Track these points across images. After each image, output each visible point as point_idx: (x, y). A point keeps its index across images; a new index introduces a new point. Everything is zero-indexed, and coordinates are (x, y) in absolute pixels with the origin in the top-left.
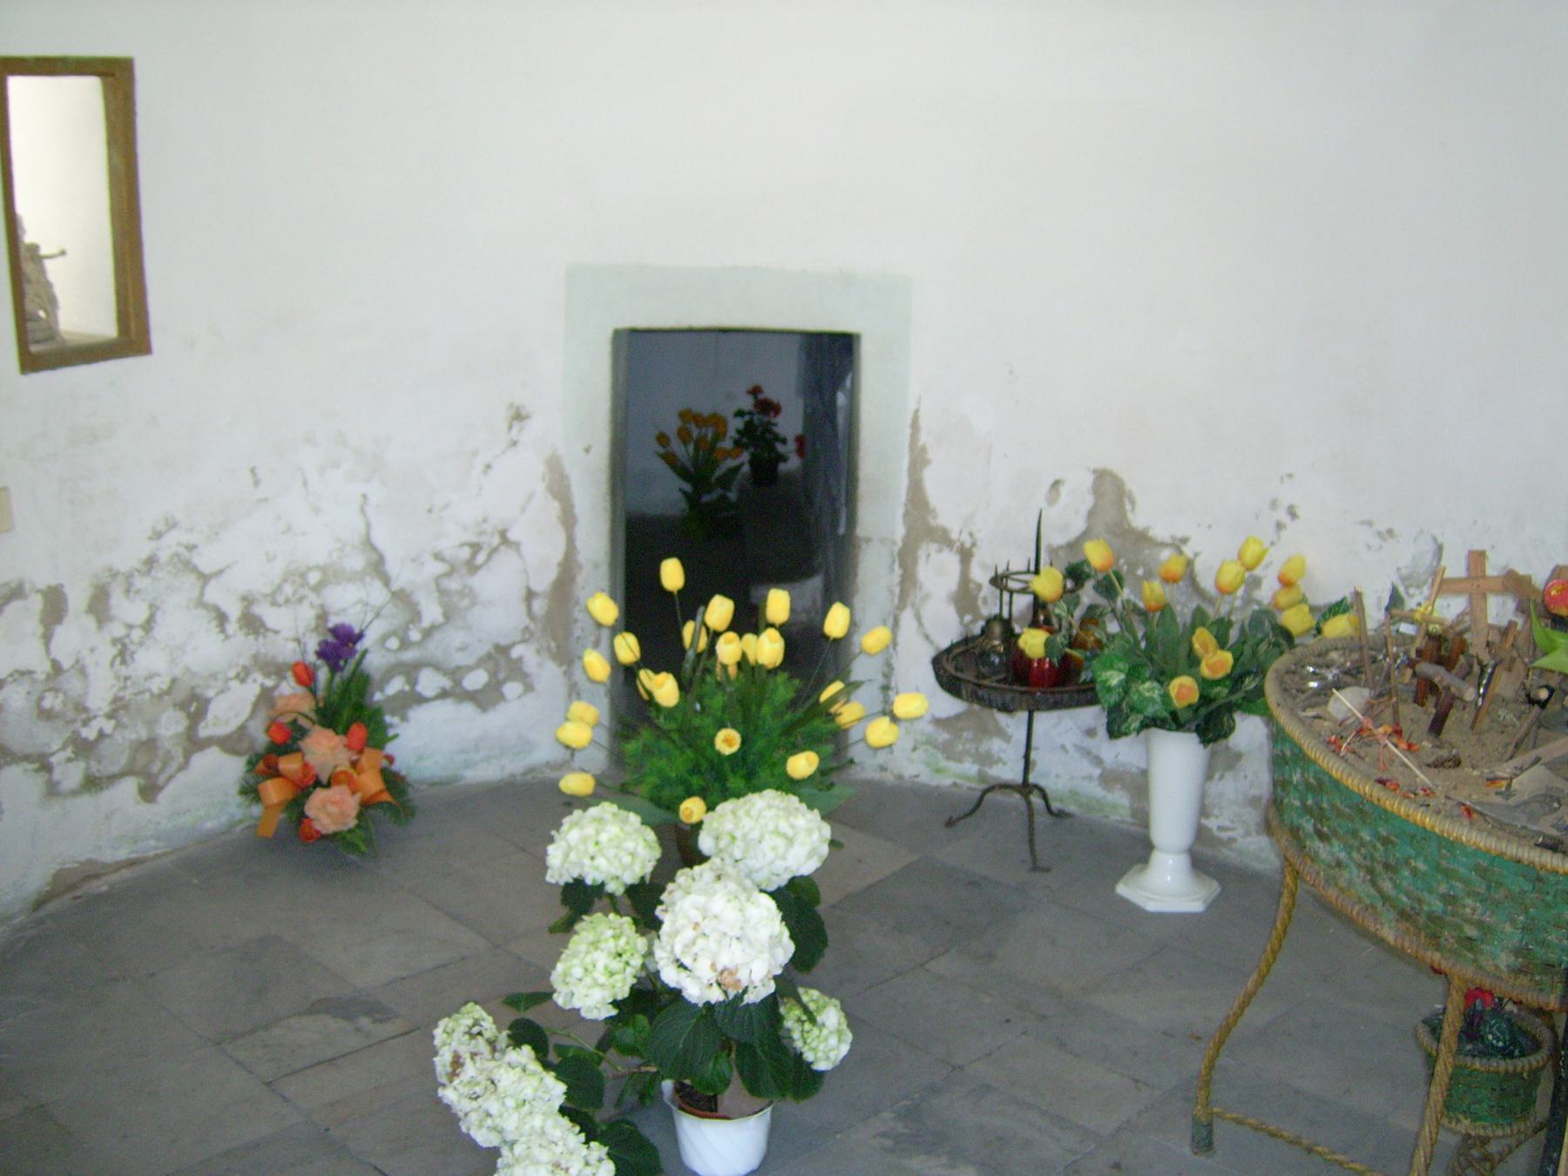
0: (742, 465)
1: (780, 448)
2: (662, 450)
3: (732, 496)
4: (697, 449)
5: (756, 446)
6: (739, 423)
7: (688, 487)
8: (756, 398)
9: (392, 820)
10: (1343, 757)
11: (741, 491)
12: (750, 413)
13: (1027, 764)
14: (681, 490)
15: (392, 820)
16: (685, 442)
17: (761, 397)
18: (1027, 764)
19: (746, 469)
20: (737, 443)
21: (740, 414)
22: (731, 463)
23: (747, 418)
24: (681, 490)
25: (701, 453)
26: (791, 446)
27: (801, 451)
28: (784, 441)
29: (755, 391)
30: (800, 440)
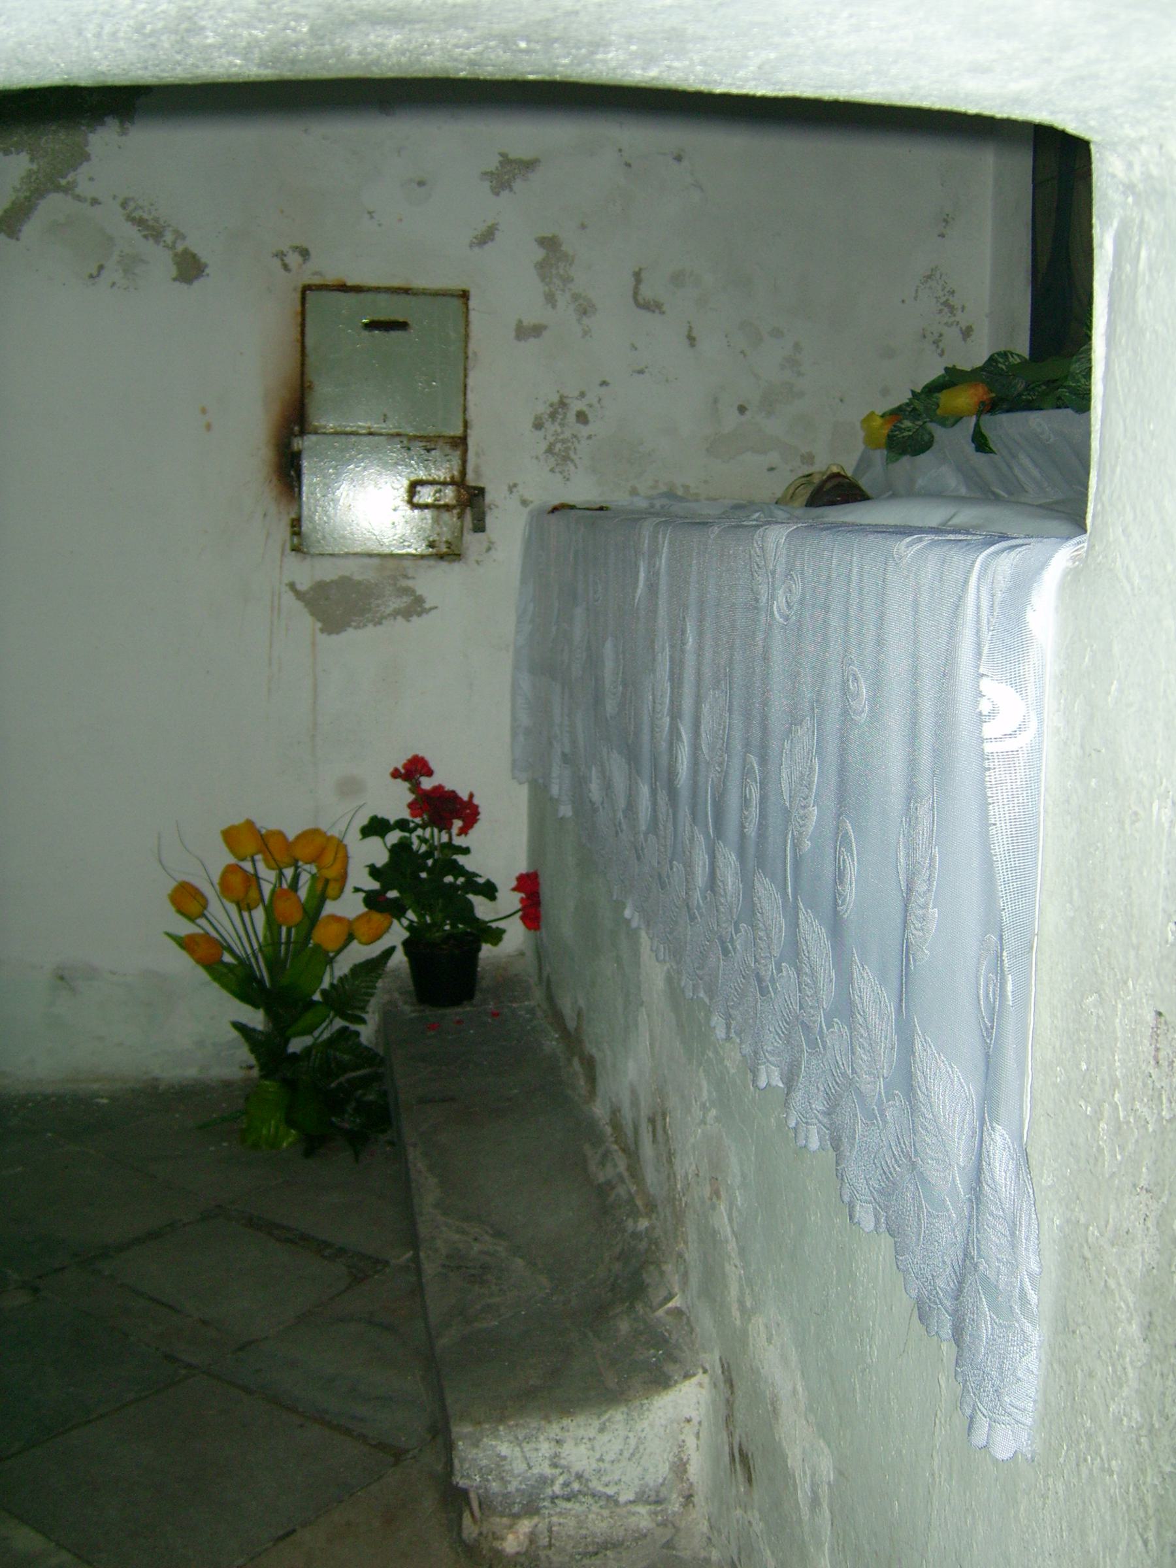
0: (389, 952)
1: (482, 908)
2: (185, 928)
3: (367, 1033)
4: (272, 923)
5: (421, 909)
6: (377, 851)
7: (256, 1018)
8: (416, 788)
9: (605, 74)
10: (837, 1169)
11: (389, 1017)
12: (402, 825)
13: (174, 879)
14: (239, 1027)
15: (605, 74)
16: (245, 906)
17: (427, 784)
18: (174, 879)
19: (399, 958)
20: (373, 901)
21: (376, 827)
22: (359, 953)
23: (394, 837)
24: (239, 1027)
25: (750, 1141)
26: (509, 900)
27: (531, 914)
28: (489, 890)
29: (415, 769)
30: (528, 884)
